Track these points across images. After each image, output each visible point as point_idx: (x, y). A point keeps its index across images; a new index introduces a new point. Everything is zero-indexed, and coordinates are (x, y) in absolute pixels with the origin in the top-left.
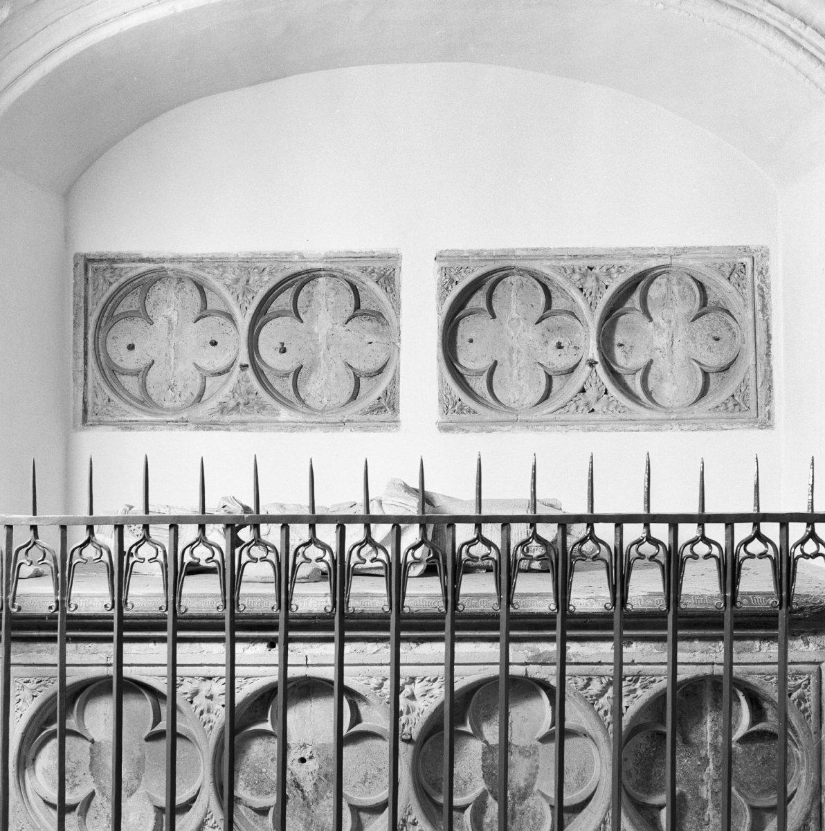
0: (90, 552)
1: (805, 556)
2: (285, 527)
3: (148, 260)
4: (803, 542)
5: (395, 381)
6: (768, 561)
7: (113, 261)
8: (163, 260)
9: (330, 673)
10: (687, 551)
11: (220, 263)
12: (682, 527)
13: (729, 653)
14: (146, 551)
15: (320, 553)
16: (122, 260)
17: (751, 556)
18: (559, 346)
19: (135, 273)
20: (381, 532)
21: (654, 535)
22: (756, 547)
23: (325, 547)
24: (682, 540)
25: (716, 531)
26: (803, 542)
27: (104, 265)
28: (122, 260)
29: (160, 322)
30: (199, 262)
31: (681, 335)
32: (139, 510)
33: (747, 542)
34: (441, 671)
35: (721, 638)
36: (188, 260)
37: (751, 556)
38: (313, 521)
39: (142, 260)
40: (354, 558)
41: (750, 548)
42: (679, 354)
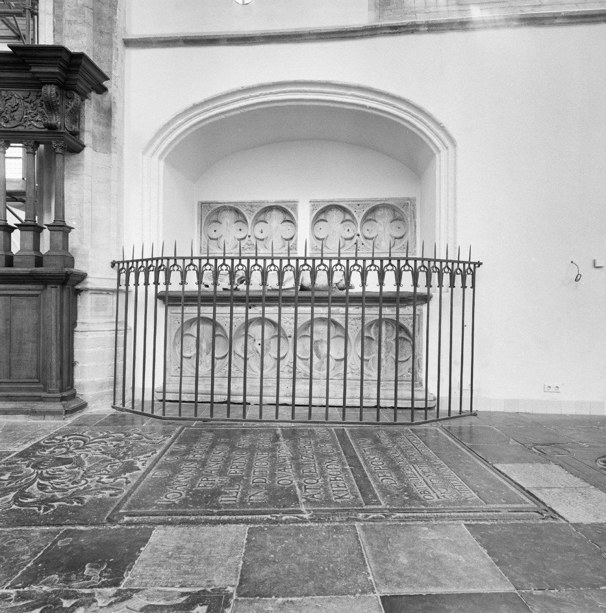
0: (407, 268)
1: (405, 270)
2: (415, 261)
3: (220, 203)
4: (404, 266)
5: (296, 241)
6: (393, 272)
7: (210, 203)
8: (225, 203)
9: (211, 316)
10: (368, 269)
11: (243, 204)
12: (300, 261)
13: (199, 310)
14: (208, 267)
15: (258, 268)
16: (212, 203)
17: (388, 270)
18: (348, 230)
19: (217, 207)
20: (244, 262)
21: (258, 263)
22: (390, 267)
23: (260, 266)
24: (300, 265)
25: (326, 262)
26: (206, 265)
27: (207, 205)
28: (212, 203)
29: (224, 223)
30: (236, 203)
31: (388, 226)
32: (457, 259)
33: (387, 266)
34: (244, 315)
35: (180, 305)
36: (233, 203)
37: (388, 270)
38: (273, 259)
39: (219, 203)
40: (220, 269)
41: (320, 268)
42: (387, 232)
